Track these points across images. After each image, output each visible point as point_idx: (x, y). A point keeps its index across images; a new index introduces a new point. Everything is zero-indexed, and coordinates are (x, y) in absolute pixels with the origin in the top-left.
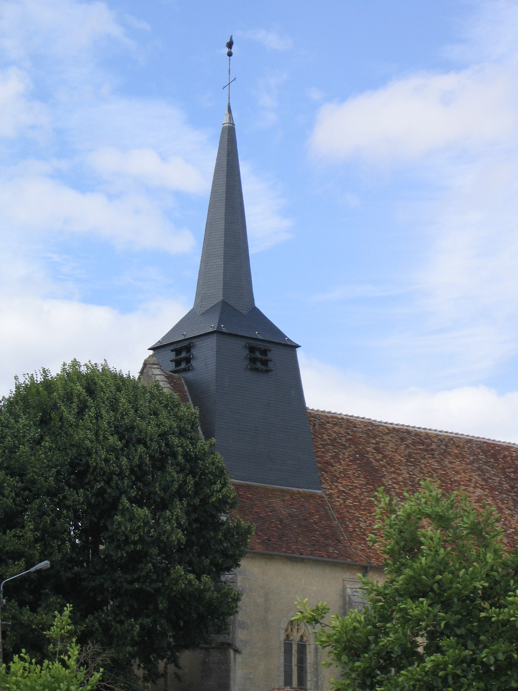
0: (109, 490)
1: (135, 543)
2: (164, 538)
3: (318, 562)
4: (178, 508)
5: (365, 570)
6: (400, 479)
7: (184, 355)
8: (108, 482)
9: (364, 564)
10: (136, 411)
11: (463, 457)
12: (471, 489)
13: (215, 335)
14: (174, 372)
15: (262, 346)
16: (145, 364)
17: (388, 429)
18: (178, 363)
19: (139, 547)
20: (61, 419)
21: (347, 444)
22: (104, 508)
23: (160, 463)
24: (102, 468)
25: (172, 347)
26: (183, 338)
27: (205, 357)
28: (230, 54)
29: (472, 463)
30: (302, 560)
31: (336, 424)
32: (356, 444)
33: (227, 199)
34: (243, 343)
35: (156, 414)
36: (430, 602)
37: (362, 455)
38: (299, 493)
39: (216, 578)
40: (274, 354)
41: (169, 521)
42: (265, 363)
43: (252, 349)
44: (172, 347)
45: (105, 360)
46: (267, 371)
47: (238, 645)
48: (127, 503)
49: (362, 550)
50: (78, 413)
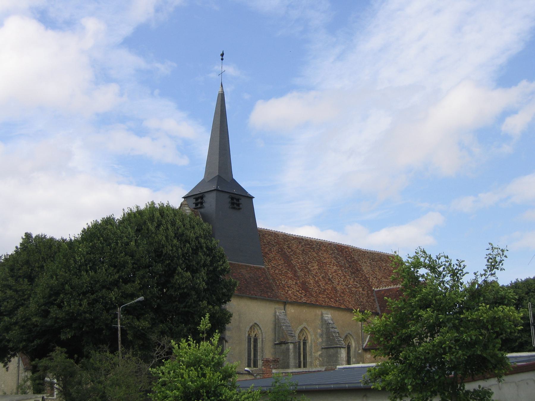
0: (172, 264)
1: (183, 289)
2: (197, 286)
3: (264, 300)
4: (203, 273)
5: (285, 303)
6: (300, 261)
7: (199, 200)
8: (172, 261)
9: (285, 300)
10: (184, 226)
11: (328, 251)
12: (332, 266)
13: (215, 192)
14: (195, 209)
15: (237, 197)
16: (181, 205)
17: (293, 237)
18: (196, 204)
19: (185, 290)
20: (148, 229)
21: (275, 244)
22: (171, 272)
23: (195, 251)
24: (169, 254)
25: (194, 197)
26: (199, 192)
27: (210, 202)
28: (222, 59)
29: (331, 254)
30: (256, 299)
31: (269, 235)
32: (279, 244)
33: (220, 126)
34: (227, 196)
35: (194, 228)
36: (432, 310)
37: (282, 249)
38: (254, 267)
39: (220, 306)
40: (243, 201)
41: (199, 278)
42: (238, 205)
43: (232, 199)
44: (194, 197)
45: (490, 244)
46: (239, 209)
47: (227, 338)
48: (180, 270)
49: (283, 294)
50: (156, 227)
